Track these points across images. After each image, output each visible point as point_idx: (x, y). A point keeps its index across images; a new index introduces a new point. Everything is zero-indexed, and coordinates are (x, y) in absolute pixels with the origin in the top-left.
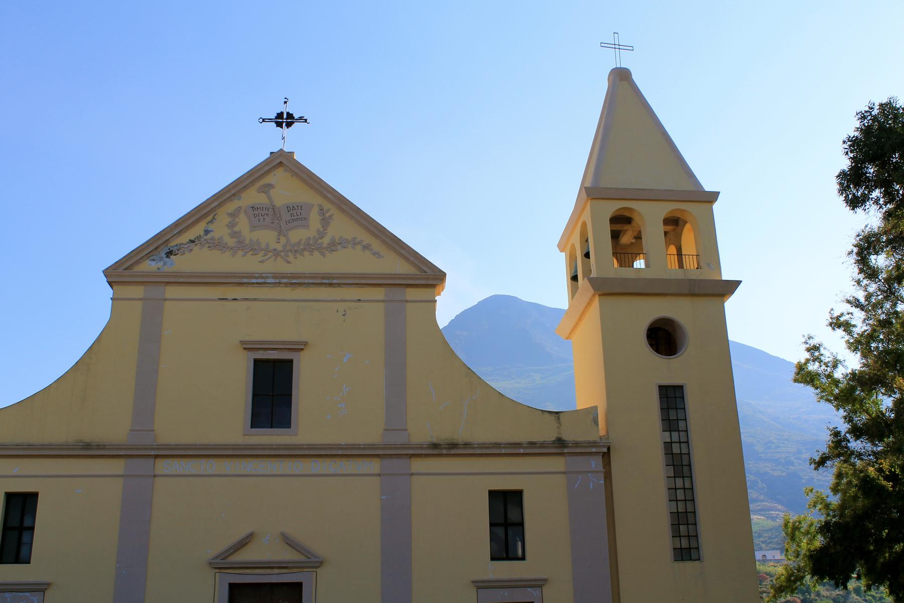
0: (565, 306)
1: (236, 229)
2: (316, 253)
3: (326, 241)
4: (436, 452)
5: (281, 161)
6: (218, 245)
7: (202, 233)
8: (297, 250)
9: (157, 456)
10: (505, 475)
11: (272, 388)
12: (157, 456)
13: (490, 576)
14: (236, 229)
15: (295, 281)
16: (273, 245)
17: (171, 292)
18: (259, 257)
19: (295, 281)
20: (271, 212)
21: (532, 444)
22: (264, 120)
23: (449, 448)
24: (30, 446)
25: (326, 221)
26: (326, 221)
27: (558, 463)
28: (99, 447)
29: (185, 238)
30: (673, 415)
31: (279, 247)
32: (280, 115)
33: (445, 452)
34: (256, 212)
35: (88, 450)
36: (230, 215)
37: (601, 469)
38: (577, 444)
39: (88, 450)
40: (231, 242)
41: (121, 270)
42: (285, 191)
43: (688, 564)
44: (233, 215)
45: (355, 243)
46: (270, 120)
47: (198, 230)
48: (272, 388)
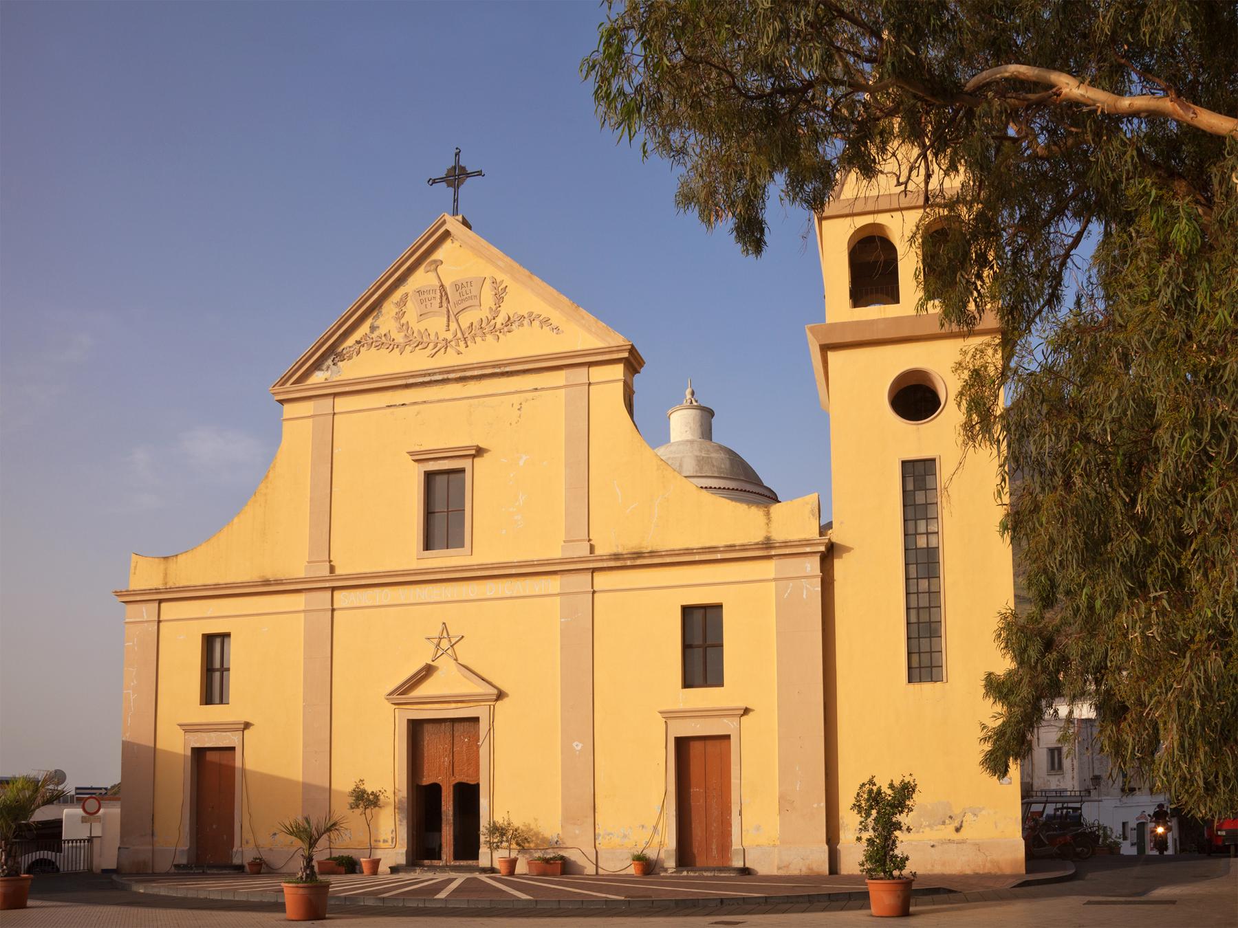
0: (829, 320)
1: (403, 321)
2: (489, 337)
3: (500, 320)
4: (618, 564)
7: (368, 331)
8: (466, 337)
9: (335, 395)
10: (699, 585)
11: (443, 502)
12: (335, 395)
13: (681, 706)
14: (403, 321)
15: (464, 376)
16: (444, 335)
17: (342, 404)
18: (429, 351)
19: (464, 376)
21: (731, 548)
22: (434, 182)
23: (634, 558)
24: (217, 586)
25: (499, 298)
26: (499, 298)
27: (768, 569)
28: (278, 582)
29: (350, 341)
30: (920, 498)
31: (449, 336)
33: (629, 563)
34: (423, 297)
35: (269, 587)
36: (397, 304)
37: (818, 572)
38: (786, 544)
39: (269, 587)
40: (399, 338)
41: (288, 385)
43: (927, 687)
44: (403, 301)
45: (532, 318)
46: (442, 180)
47: (364, 328)
48: (443, 502)
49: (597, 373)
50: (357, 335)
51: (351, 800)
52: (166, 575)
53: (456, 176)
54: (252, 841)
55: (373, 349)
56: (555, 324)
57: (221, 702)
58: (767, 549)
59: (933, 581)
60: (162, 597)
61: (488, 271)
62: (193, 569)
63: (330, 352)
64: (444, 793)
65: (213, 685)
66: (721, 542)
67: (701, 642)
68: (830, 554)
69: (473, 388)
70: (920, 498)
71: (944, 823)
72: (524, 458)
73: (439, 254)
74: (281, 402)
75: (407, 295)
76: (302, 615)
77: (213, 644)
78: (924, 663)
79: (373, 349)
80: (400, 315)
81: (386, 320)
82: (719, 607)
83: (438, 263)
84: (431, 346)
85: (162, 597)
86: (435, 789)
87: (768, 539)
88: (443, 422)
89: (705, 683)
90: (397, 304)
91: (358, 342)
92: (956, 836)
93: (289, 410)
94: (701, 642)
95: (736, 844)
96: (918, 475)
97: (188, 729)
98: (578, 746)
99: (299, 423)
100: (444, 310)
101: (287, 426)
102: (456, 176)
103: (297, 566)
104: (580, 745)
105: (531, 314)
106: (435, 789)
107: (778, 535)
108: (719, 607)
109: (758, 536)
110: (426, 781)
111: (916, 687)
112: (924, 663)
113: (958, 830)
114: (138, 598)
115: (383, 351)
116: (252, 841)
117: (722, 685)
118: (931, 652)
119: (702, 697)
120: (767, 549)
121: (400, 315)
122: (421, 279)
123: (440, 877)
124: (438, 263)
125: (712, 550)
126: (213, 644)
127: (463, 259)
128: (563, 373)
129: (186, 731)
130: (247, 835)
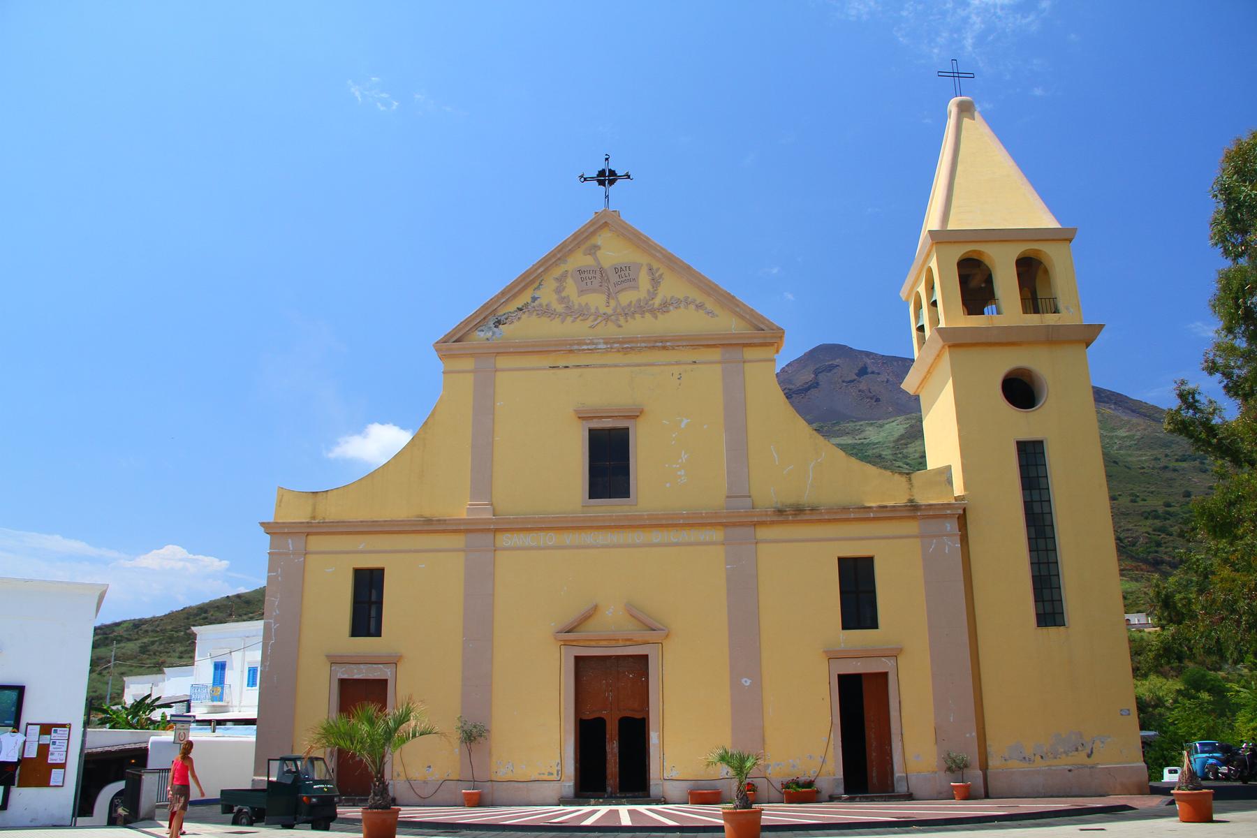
1: (563, 294)
3: (657, 302)
5: (604, 222)
6: (547, 312)
14: (563, 294)
16: (603, 310)
18: (589, 323)
20: (598, 275)
25: (655, 282)
27: (912, 527)
31: (609, 311)
32: (602, 173)
39: (429, 526)
40: (560, 308)
42: (612, 252)
43: (1052, 631)
44: (561, 279)
45: (687, 302)
47: (525, 298)
50: (519, 303)
52: (314, 509)
54: (403, 774)
59: (1045, 504)
64: (609, 727)
67: (858, 592)
70: (1037, 509)
71: (1077, 750)
72: (685, 421)
78: (1049, 612)
80: (558, 291)
81: (547, 295)
83: (597, 247)
86: (600, 723)
87: (911, 501)
88: (607, 388)
89: (369, 634)
91: (520, 309)
92: (1089, 761)
94: (858, 592)
95: (898, 773)
96: (1031, 455)
98: (747, 682)
104: (749, 682)
106: (600, 723)
107: (922, 500)
109: (901, 500)
110: (588, 716)
111: (1044, 630)
112: (1049, 612)
113: (1089, 756)
116: (403, 774)
118: (1039, 563)
119: (860, 637)
124: (597, 247)
130: (398, 768)
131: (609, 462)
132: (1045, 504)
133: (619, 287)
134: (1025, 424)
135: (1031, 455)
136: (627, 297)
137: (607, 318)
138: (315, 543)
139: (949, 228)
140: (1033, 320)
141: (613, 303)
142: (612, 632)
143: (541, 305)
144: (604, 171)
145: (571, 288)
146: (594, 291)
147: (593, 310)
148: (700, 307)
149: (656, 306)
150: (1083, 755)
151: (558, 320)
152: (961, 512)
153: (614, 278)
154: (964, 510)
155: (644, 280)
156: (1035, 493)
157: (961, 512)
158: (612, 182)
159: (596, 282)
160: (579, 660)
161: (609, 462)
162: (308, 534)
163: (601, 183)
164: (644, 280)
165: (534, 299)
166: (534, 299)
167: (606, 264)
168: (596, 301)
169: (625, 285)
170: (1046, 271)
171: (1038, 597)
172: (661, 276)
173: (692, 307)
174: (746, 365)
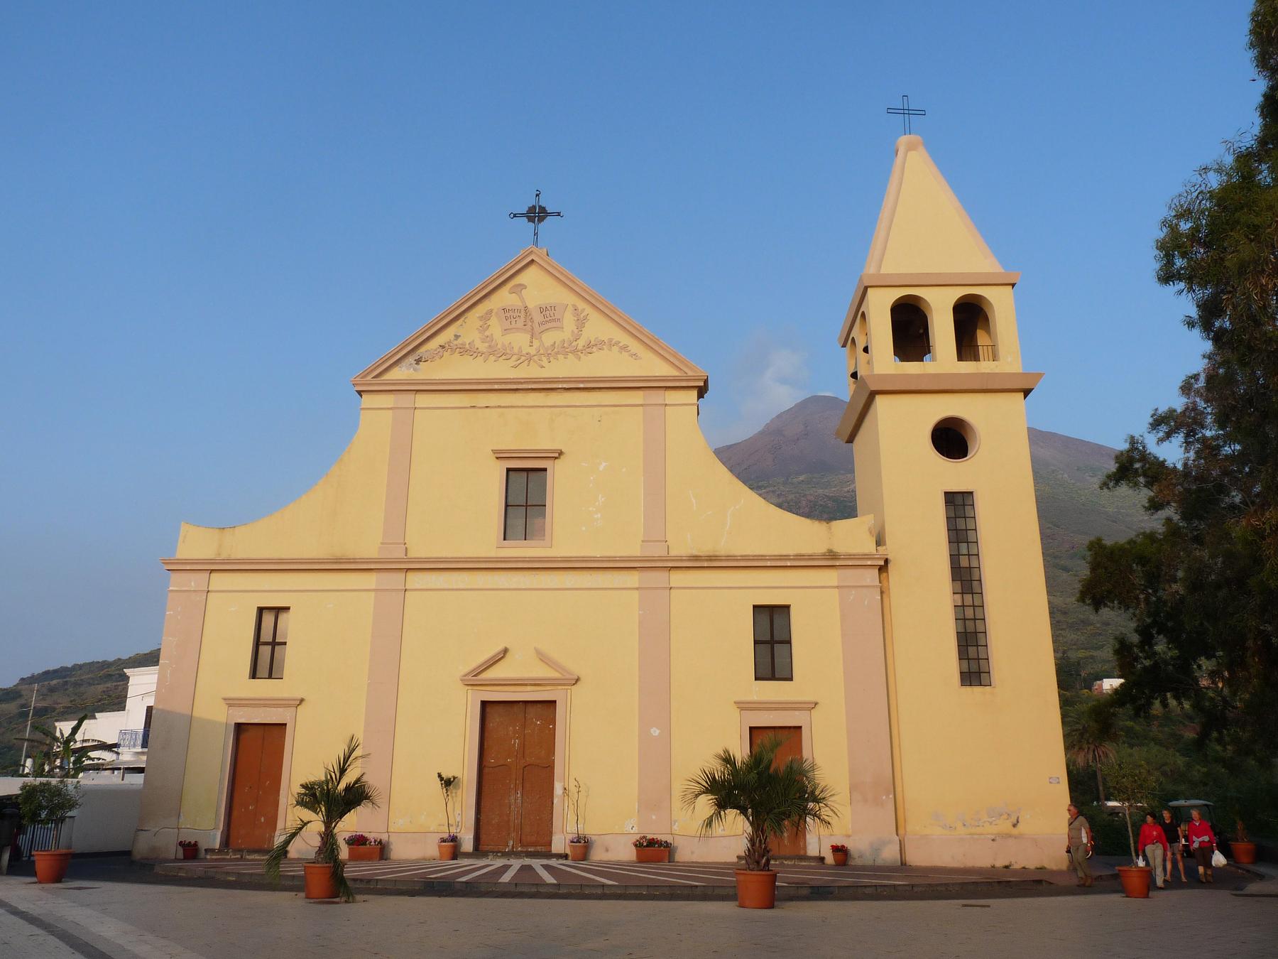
1: (487, 333)
3: (581, 343)
6: (464, 351)
8: (551, 353)
18: (512, 362)
25: (581, 323)
27: (831, 577)
31: (532, 351)
36: (481, 318)
40: (483, 347)
41: (369, 378)
45: (611, 344)
46: (522, 215)
49: (672, 397)
51: (1112, 467)
53: (537, 214)
55: (457, 355)
56: (633, 351)
57: (270, 677)
58: (831, 560)
60: (214, 567)
61: (570, 299)
62: (248, 541)
63: (412, 351)
65: (266, 654)
66: (791, 552)
67: (772, 637)
68: (883, 568)
69: (483, 399)
73: (523, 278)
74: (360, 393)
75: (491, 311)
76: (373, 594)
77: (270, 614)
78: (974, 670)
79: (457, 355)
82: (786, 609)
83: (522, 286)
84: (514, 358)
85: (214, 567)
90: (481, 318)
91: (442, 347)
93: (367, 400)
94: (772, 637)
96: (959, 505)
97: (231, 703)
98: (655, 732)
99: (377, 416)
100: (528, 327)
101: (365, 417)
102: (537, 214)
103: (369, 547)
105: (610, 340)
107: (839, 549)
108: (786, 609)
109: (821, 549)
112: (974, 670)
113: (1014, 826)
114: (188, 567)
115: (467, 358)
117: (790, 678)
119: (772, 690)
120: (831, 560)
121: (484, 328)
122: (505, 297)
123: (499, 863)
124: (522, 286)
125: (786, 558)
126: (270, 614)
127: (537, 287)
128: (641, 393)
129: (230, 705)
131: (525, 492)
132: (974, 559)
133: (543, 327)
134: (955, 474)
135: (959, 505)
136: (549, 338)
137: (530, 358)
138: (218, 581)
139: (882, 271)
140: (968, 367)
141: (536, 343)
142: (521, 673)
143: (464, 344)
144: (534, 207)
145: (495, 328)
146: (518, 329)
147: (516, 350)
148: (624, 348)
149: (580, 347)
150: (1009, 824)
151: (480, 359)
152: (882, 563)
153: (538, 318)
154: (886, 561)
155: (569, 322)
156: (963, 547)
157: (882, 563)
158: (541, 219)
159: (520, 323)
160: (484, 704)
161: (525, 492)
162: (212, 571)
163: (531, 220)
164: (569, 322)
165: (457, 337)
166: (457, 337)
167: (531, 305)
168: (520, 340)
169: (550, 325)
170: (986, 319)
171: (963, 653)
172: (585, 318)
173: (615, 349)
174: (529, 336)
